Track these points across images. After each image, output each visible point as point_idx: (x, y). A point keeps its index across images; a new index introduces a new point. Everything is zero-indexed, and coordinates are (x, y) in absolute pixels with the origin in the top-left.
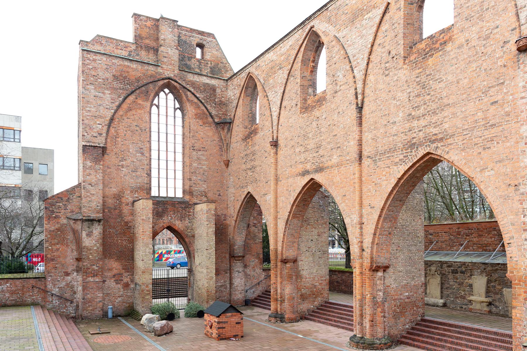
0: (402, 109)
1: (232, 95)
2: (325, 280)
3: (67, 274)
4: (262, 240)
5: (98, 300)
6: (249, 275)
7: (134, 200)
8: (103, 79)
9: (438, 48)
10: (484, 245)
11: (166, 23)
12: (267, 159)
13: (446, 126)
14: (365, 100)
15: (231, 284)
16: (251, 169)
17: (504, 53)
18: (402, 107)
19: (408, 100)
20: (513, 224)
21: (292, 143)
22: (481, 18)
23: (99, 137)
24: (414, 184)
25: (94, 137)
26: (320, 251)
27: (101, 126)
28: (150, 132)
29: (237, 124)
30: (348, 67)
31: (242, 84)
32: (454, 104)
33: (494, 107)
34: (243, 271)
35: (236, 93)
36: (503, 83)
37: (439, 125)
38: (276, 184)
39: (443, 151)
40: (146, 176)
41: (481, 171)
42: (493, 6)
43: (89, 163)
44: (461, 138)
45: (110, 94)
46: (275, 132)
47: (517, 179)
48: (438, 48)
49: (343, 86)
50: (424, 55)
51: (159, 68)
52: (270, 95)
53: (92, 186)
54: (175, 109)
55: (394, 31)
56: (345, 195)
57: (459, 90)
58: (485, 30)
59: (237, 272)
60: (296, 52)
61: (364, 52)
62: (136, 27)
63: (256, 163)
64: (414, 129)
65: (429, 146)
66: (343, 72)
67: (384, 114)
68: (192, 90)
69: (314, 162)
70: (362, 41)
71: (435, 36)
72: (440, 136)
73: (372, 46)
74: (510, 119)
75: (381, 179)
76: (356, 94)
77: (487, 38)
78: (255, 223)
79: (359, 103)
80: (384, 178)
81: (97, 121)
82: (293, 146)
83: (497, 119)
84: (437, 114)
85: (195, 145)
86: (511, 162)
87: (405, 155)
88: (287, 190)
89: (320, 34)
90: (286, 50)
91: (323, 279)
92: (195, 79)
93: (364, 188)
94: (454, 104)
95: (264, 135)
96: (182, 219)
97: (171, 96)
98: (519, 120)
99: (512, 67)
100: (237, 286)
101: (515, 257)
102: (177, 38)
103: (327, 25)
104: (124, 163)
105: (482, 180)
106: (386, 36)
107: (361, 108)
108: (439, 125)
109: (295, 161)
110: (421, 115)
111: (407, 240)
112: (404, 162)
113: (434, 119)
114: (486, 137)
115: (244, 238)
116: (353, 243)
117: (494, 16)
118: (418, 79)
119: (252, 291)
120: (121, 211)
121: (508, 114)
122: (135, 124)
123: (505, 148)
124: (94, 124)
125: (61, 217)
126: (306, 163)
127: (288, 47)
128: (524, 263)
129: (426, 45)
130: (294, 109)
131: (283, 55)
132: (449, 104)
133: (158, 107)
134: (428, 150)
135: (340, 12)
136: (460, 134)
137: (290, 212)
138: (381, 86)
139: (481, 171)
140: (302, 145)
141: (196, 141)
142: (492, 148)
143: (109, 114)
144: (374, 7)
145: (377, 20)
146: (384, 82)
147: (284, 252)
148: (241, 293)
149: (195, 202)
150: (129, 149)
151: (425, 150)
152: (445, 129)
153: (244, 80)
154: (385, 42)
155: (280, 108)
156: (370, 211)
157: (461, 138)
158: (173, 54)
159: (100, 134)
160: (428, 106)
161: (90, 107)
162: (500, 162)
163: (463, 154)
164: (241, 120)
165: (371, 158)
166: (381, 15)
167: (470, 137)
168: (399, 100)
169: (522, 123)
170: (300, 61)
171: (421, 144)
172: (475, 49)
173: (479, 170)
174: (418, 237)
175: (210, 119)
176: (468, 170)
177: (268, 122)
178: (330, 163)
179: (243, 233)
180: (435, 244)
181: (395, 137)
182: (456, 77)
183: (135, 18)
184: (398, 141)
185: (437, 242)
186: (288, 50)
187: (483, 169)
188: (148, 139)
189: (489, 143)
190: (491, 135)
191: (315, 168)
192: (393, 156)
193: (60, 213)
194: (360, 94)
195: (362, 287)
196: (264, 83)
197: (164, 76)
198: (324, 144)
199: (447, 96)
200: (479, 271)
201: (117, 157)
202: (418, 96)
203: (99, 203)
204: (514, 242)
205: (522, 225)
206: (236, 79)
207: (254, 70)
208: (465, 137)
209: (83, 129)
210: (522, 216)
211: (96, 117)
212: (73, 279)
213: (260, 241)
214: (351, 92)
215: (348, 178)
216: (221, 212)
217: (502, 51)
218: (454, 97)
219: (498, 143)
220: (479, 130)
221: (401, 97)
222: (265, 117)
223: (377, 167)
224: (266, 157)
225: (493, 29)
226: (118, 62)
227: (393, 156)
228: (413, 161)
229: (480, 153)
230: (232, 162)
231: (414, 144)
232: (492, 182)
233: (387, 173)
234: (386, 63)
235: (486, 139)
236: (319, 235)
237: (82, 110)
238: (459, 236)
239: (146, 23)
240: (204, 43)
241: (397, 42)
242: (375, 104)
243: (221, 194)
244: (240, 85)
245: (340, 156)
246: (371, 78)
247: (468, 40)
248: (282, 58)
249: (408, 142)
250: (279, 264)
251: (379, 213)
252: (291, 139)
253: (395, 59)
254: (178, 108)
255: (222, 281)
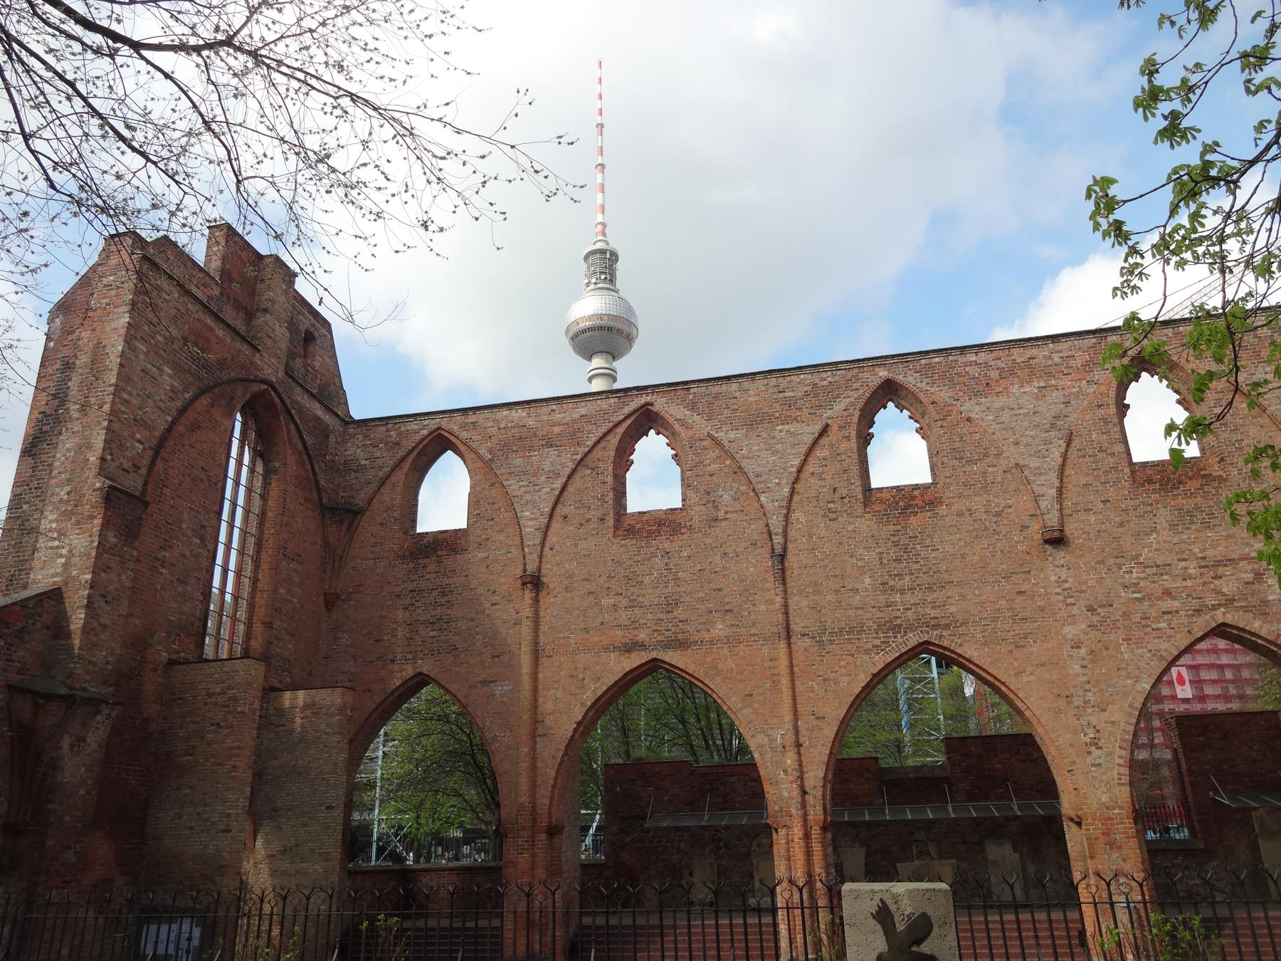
11: (280, 270)
13: (953, 609)
14: (790, 546)
20: (1072, 746)
27: (141, 447)
36: (1029, 572)
40: (201, 598)
45: (170, 377)
51: (258, 355)
53: (106, 602)
56: (751, 695)
72: (944, 622)
80: (844, 671)
81: (138, 432)
92: (303, 402)
93: (797, 684)
94: (960, 584)
107: (783, 557)
118: (896, 539)
121: (1042, 609)
122: (201, 464)
143: (162, 422)
147: (554, 810)
157: (979, 629)
159: (137, 467)
161: (130, 394)
162: (1042, 665)
171: (911, 628)
175: (315, 496)
181: (860, 612)
197: (261, 375)
200: (848, 839)
201: (157, 536)
203: (112, 654)
219: (1035, 642)
226: (197, 312)
231: (900, 626)
246: (798, 516)
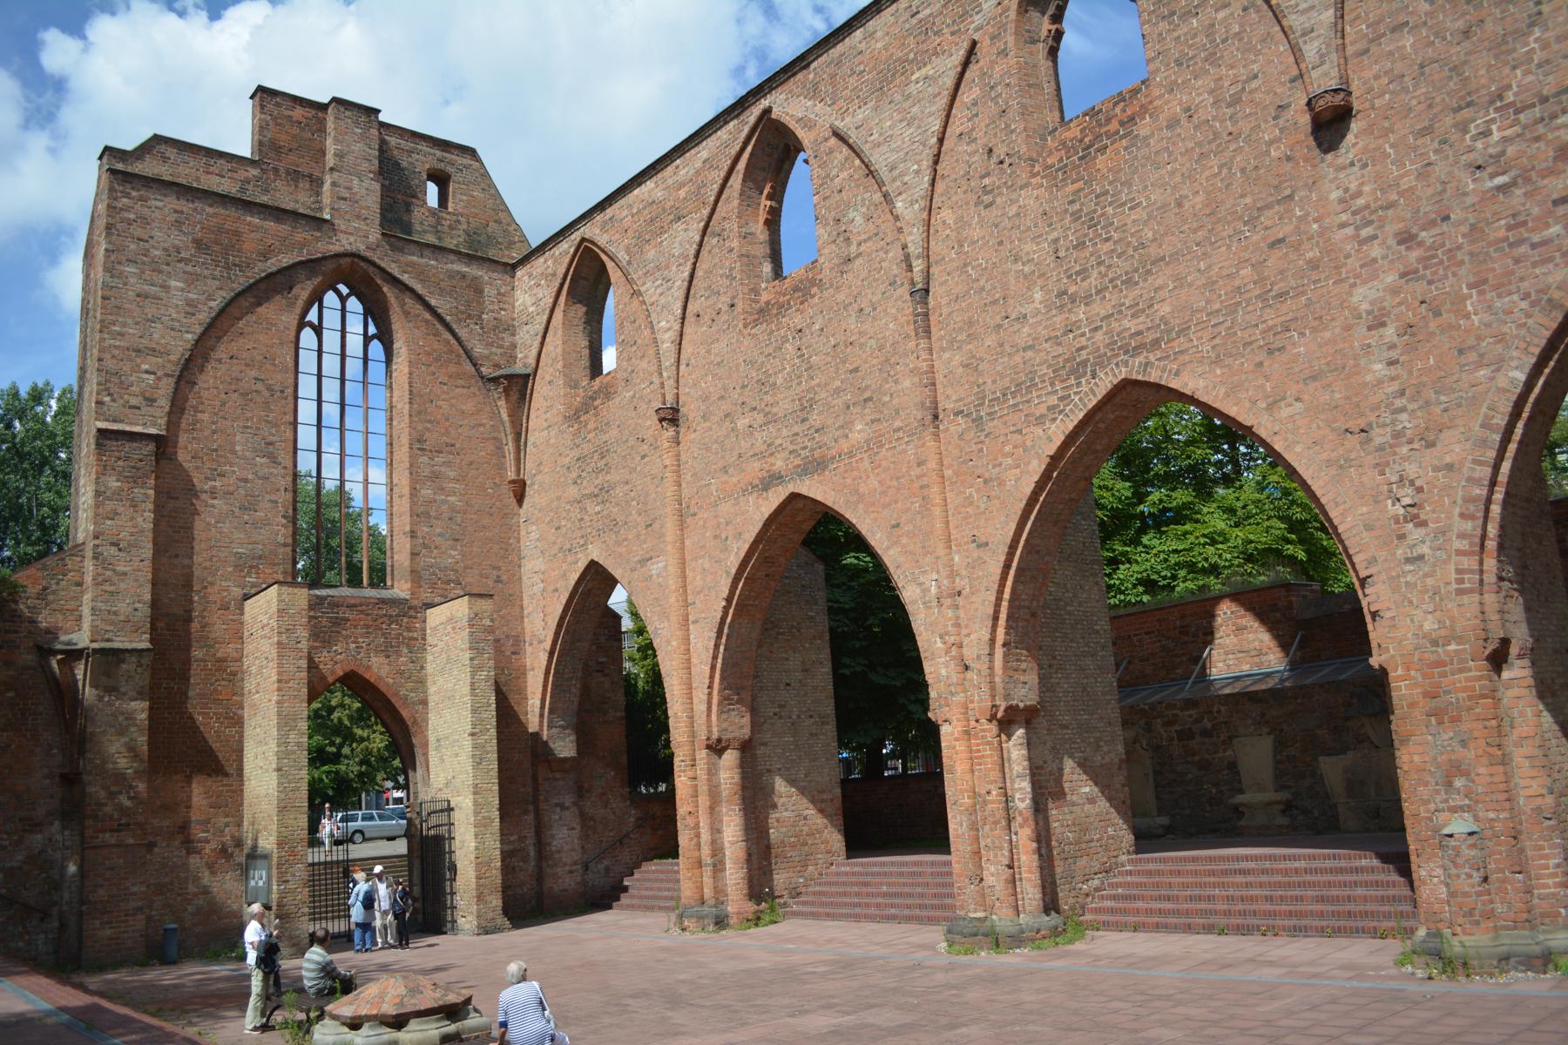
0: (1040, 282)
1: (529, 303)
2: (832, 800)
3: (34, 826)
4: (623, 714)
5: (133, 904)
6: (592, 819)
7: (245, 595)
8: (165, 250)
9: (1117, 132)
10: (1254, 653)
12: (646, 460)
13: (1165, 309)
14: (934, 270)
15: (541, 844)
16: (596, 496)
17: (1282, 130)
18: (1039, 277)
19: (1053, 258)
20: (1369, 528)
21: (725, 406)
22: (1212, 59)
23: (144, 410)
24: (1087, 475)
25: (130, 407)
26: (811, 717)
28: (296, 398)
29: (548, 378)
30: (878, 197)
31: (561, 270)
32: (1175, 256)
33: (1277, 253)
34: (575, 804)
35: (540, 295)
36: (1290, 197)
37: (1143, 311)
38: (682, 525)
39: (1164, 371)
41: (1270, 408)
42: (1237, 34)
43: (114, 483)
44: (1206, 335)
46: (670, 383)
47: (1362, 415)
48: (1117, 132)
49: (869, 244)
50: (1083, 150)
52: (650, 289)
53: (120, 550)
54: (367, 339)
55: (997, 103)
56: (897, 525)
57: (1185, 221)
58: (1226, 84)
59: (558, 810)
60: (723, 174)
61: (918, 157)
62: (264, 120)
63: (613, 477)
64: (1079, 328)
65: (1126, 364)
66: (864, 209)
67: (990, 299)
68: (418, 287)
69: (795, 447)
70: (911, 130)
71: (1101, 111)
72: (1150, 337)
73: (941, 141)
74: (1323, 276)
75: (1000, 465)
76: (907, 259)
77: (1235, 101)
78: (601, 663)
79: (918, 278)
80: (1009, 461)
82: (726, 416)
83: (1290, 279)
84: (1137, 283)
85: (427, 435)
86: (1342, 376)
87: (1060, 394)
88: (716, 537)
89: (792, 125)
90: (692, 171)
91: (825, 797)
94: (1175, 256)
95: (634, 397)
96: (388, 650)
97: (354, 304)
98: (1344, 276)
99: (1306, 160)
100: (559, 852)
101: (1389, 609)
102: (377, 153)
103: (809, 103)
104: (217, 484)
105: (1277, 429)
106: (977, 115)
108: (1143, 311)
109: (735, 454)
110: (1094, 291)
111: (1072, 641)
112: (1061, 412)
113: (1129, 297)
114: (1270, 323)
115: (576, 703)
116: (933, 654)
117: (1243, 53)
119: (602, 866)
120: (205, 626)
121: (1314, 265)
122: (254, 373)
123: (1320, 346)
124: (133, 370)
125: (18, 647)
126: (771, 454)
127: (698, 164)
128: (1412, 621)
129: (1082, 131)
130: (724, 317)
131: (684, 185)
132: (1163, 258)
133: (318, 330)
134: (1123, 373)
135: (845, 69)
136: (1203, 325)
137: (729, 600)
138: (976, 233)
139: (1270, 408)
140: (755, 409)
141: (429, 426)
142: (1289, 347)
144: (936, 54)
145: (949, 81)
146: (981, 221)
148: (570, 872)
149: (428, 601)
150: (233, 444)
151: (1115, 375)
152: (1162, 318)
153: (567, 260)
154: (973, 129)
155: (683, 318)
156: (975, 555)
158: (363, 191)
159: (151, 401)
160: (1109, 266)
162: (1314, 378)
163: (1218, 372)
164: (559, 366)
165: (967, 415)
166: (959, 69)
167: (1230, 328)
168: (1029, 261)
169: (1352, 281)
170: (736, 195)
171: (1101, 361)
172: (1211, 127)
173: (1264, 405)
174: (1097, 632)
175: (469, 367)
176: (1235, 408)
177: (646, 360)
178: (844, 445)
179: (573, 690)
180: (1126, 668)
181: (1030, 354)
182: (1173, 194)
183: (262, 99)
184: (1038, 360)
185: (1129, 662)
186: (698, 173)
187: (1275, 402)
188: (290, 418)
189: (1278, 337)
190: (1283, 318)
191: (799, 466)
192: (1028, 402)
193: (16, 632)
194: (918, 257)
195: (972, 771)
196: (629, 263)
198: (823, 395)
199: (1155, 240)
202: (1080, 245)
204: (1380, 572)
205: (1394, 526)
206: (542, 260)
207: (597, 231)
208: (1216, 330)
209: (99, 384)
210: (1389, 502)
211: (139, 351)
212: (50, 840)
213: (618, 714)
214: (891, 255)
215: (903, 477)
216: (505, 629)
217: (1276, 126)
218: (1173, 238)
219: (1302, 334)
220: (1249, 308)
221: (1035, 252)
222: (635, 348)
223: (986, 436)
224: (643, 457)
225: (1246, 82)
227: (1028, 402)
228: (1085, 405)
229: (1261, 364)
230: (533, 484)
231: (1084, 363)
232: (1302, 431)
233: (1015, 447)
234: (983, 177)
235: (1270, 329)
236: (806, 671)
237: (101, 331)
238: (1186, 639)
239: (290, 113)
240: (449, 169)
241: (1008, 126)
242: (963, 277)
243: (504, 578)
244: (554, 275)
245: (873, 421)
247: (1189, 109)
248: (682, 193)
249: (1067, 361)
250: (702, 754)
251: (1003, 558)
252: (722, 398)
253: (1006, 165)
254: (374, 337)
255: (515, 837)
